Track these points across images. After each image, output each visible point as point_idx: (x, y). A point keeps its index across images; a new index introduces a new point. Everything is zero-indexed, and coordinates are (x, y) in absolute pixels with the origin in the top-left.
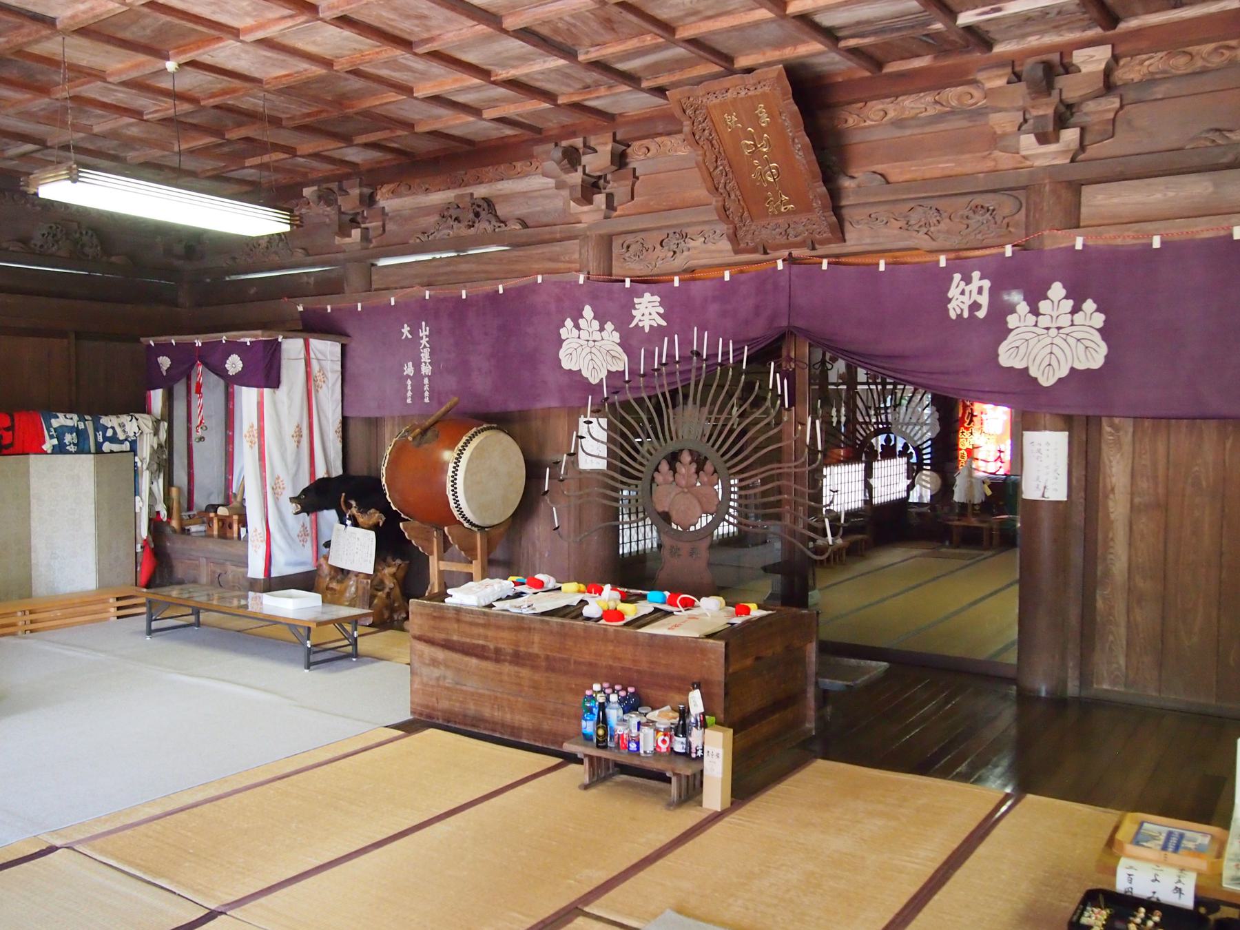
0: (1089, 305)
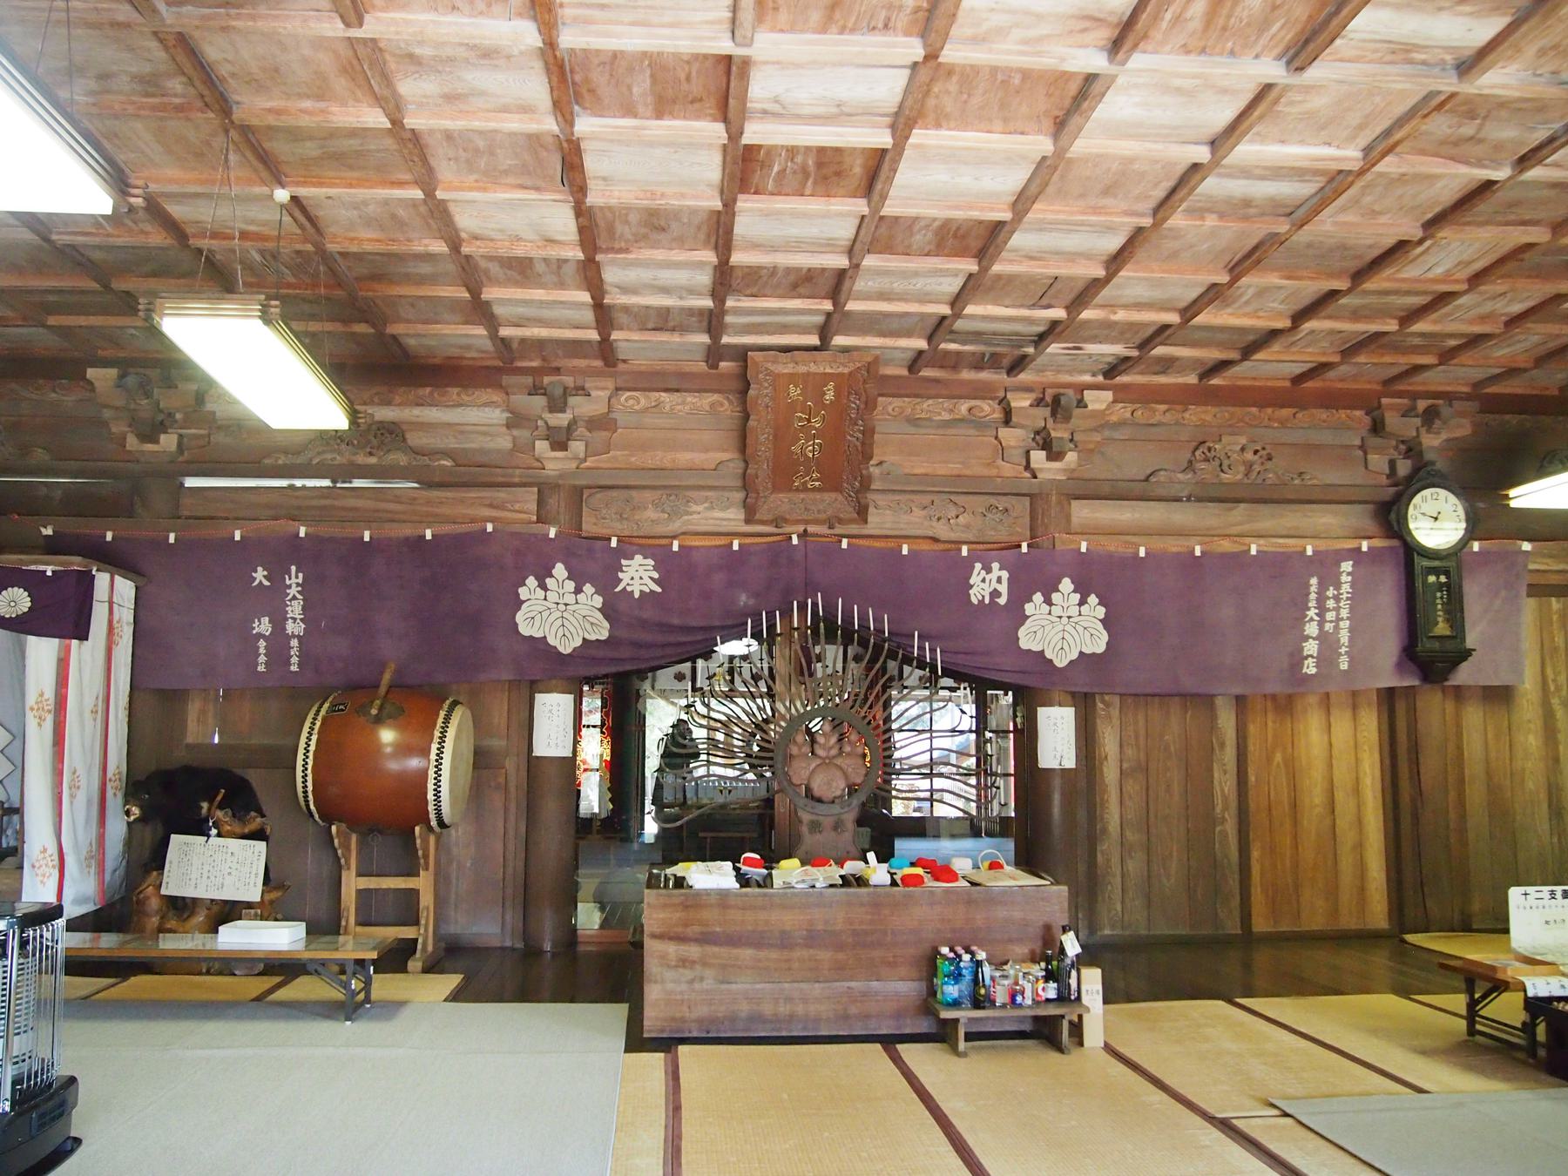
0: (1093, 599)
